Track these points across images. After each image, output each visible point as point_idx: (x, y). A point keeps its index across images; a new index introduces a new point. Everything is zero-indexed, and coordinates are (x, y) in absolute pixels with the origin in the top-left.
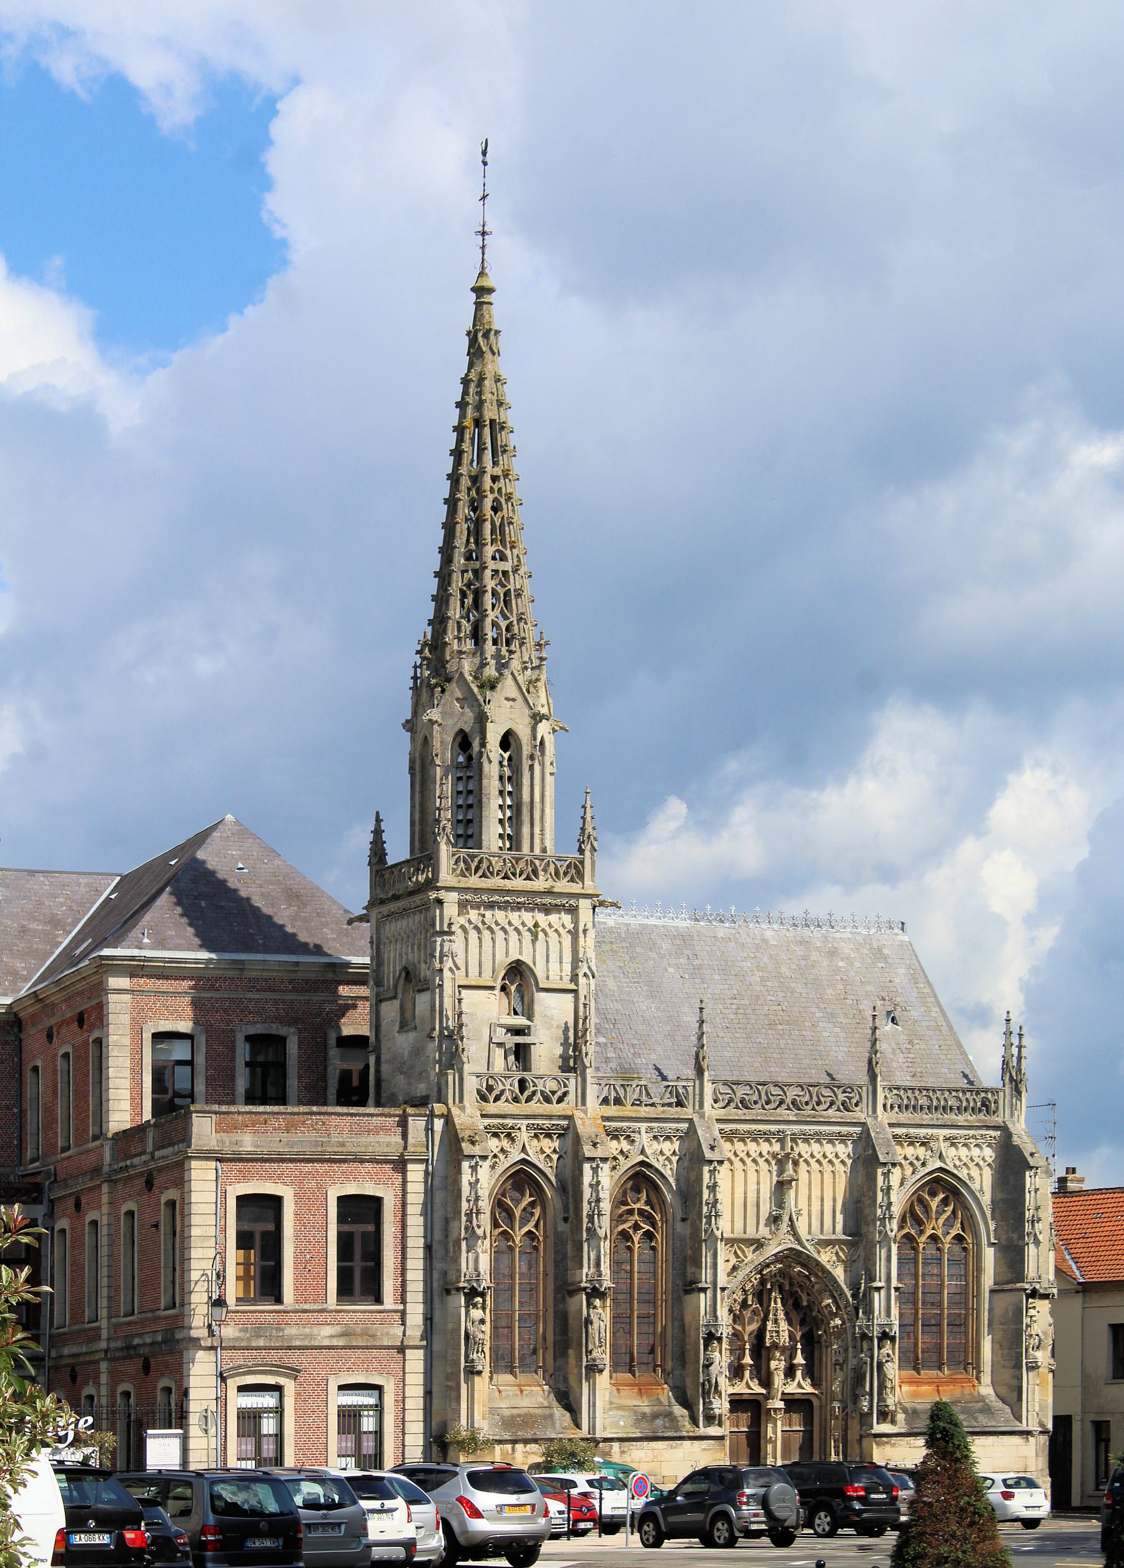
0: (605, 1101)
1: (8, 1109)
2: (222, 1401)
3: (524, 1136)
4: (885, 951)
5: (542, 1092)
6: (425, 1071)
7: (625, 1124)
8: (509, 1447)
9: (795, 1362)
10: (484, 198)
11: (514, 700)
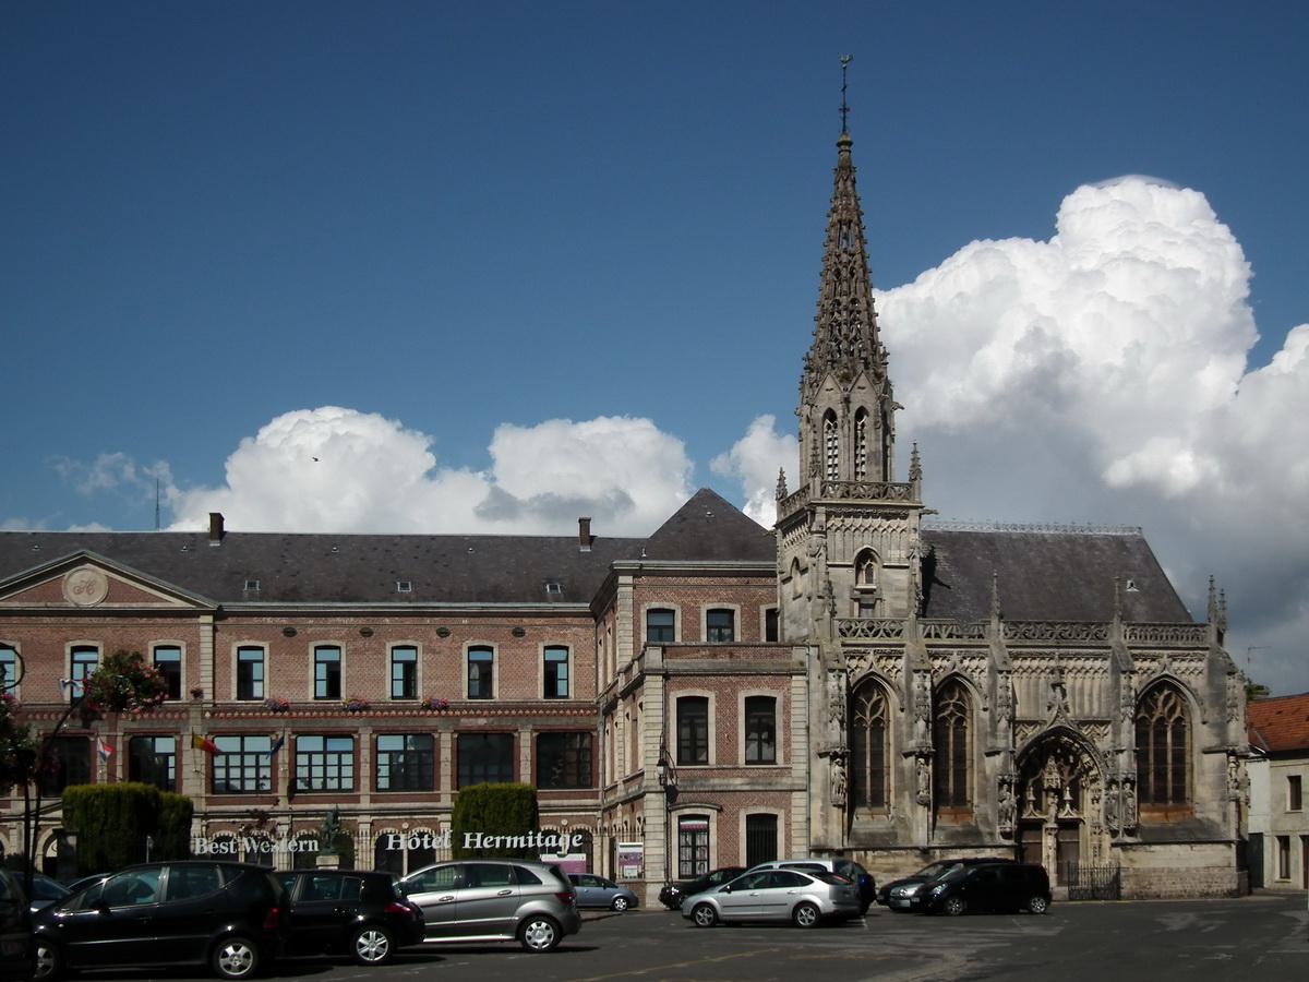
0: (929, 636)
1: (590, 665)
2: (667, 825)
3: (871, 657)
4: (1128, 545)
5: (885, 630)
8: (863, 853)
9: (1065, 798)
11: (863, 388)
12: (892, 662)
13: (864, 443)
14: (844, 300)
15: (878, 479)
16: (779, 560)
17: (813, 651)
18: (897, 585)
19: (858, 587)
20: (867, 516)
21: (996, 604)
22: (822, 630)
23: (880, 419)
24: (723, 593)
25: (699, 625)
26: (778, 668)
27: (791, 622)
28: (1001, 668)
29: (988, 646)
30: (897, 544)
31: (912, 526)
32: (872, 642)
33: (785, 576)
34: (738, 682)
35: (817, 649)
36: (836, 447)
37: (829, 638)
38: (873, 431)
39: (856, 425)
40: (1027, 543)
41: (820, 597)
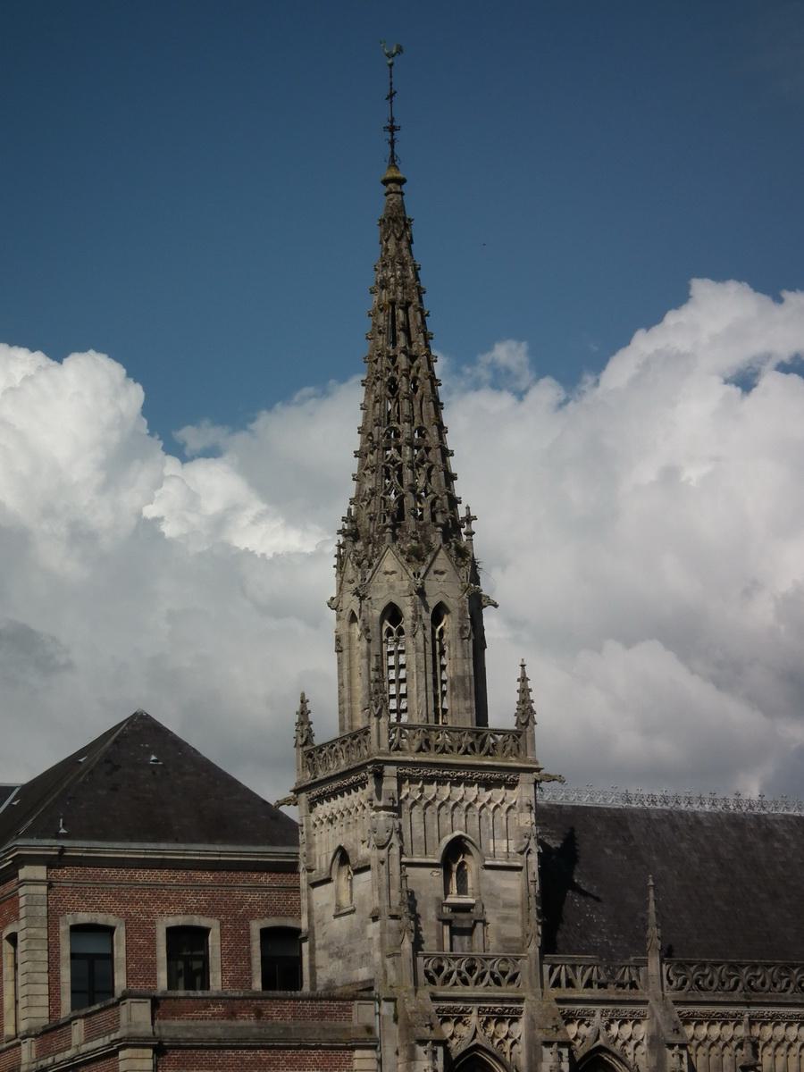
0: (557, 984)
3: (474, 1019)
5: (492, 974)
6: (368, 954)
7: (579, 1007)
10: (391, 96)
12: (505, 1027)
13: (444, 661)
14: (405, 428)
15: (468, 722)
16: (302, 850)
17: (387, 1009)
18: (506, 892)
19: (450, 900)
20: (457, 783)
21: (654, 932)
22: (397, 975)
23: (469, 624)
24: (191, 900)
25: (154, 953)
26: (330, 1036)
27: (331, 956)
28: (672, 1039)
29: (645, 1002)
30: (505, 827)
31: (525, 800)
32: (474, 994)
33: (315, 876)
34: (270, 1061)
35: (391, 1005)
36: (403, 666)
37: (411, 986)
38: (459, 641)
39: (433, 632)
40: (674, 827)
41: (394, 917)
